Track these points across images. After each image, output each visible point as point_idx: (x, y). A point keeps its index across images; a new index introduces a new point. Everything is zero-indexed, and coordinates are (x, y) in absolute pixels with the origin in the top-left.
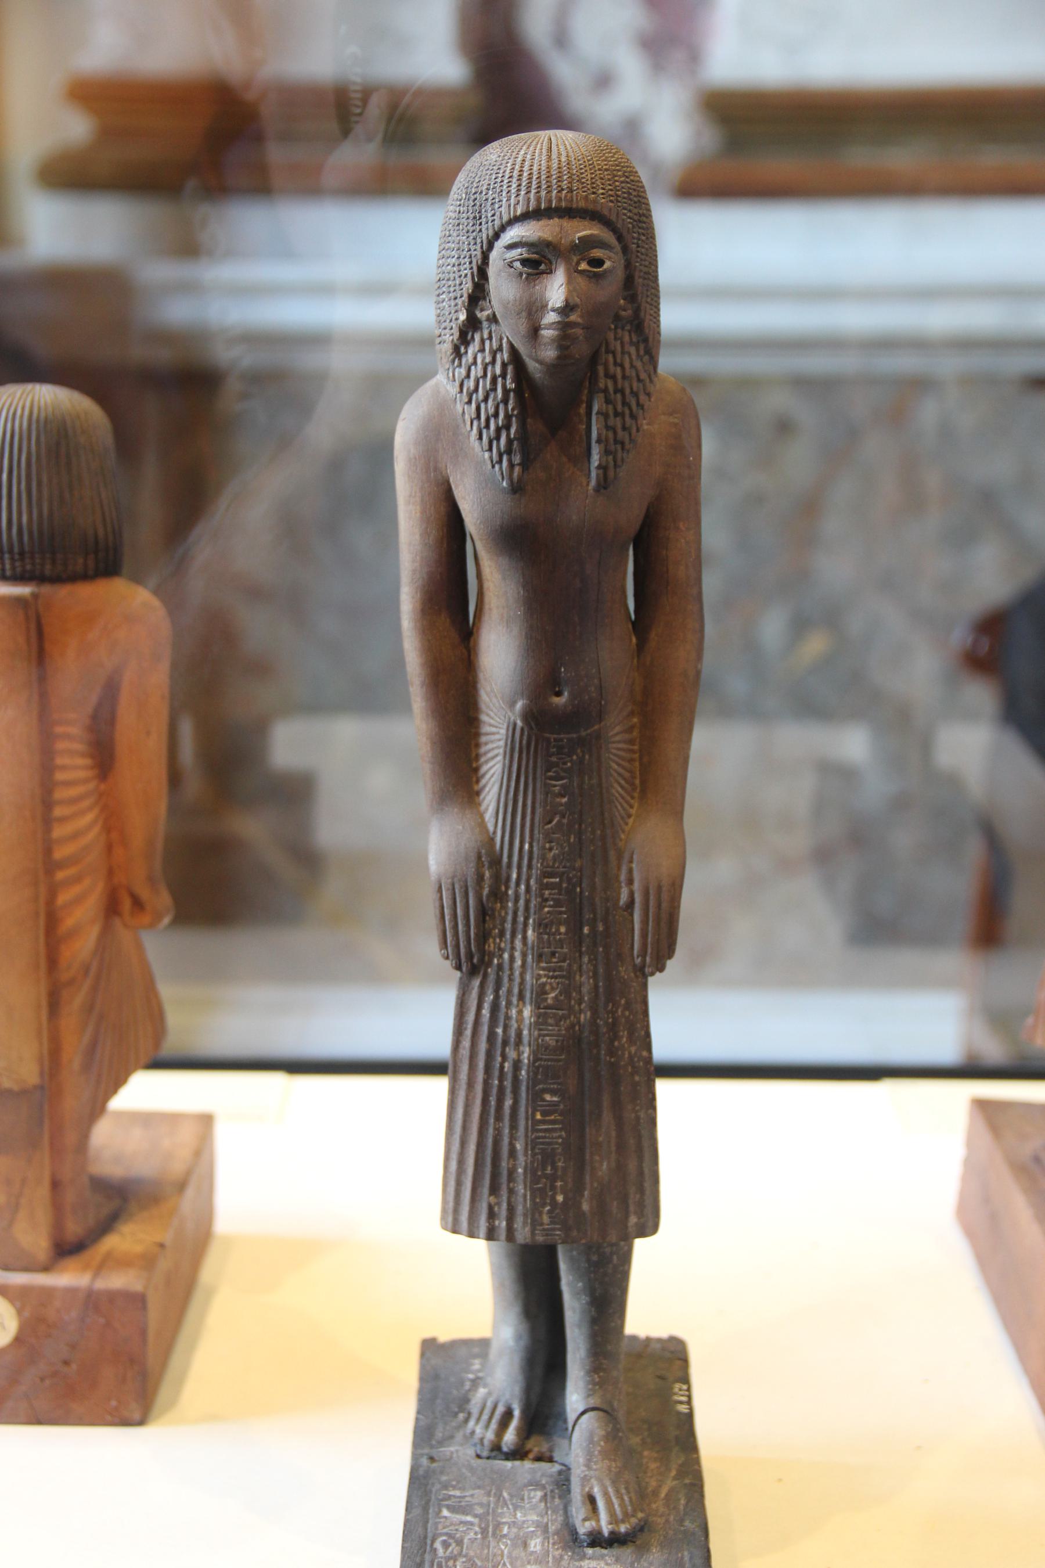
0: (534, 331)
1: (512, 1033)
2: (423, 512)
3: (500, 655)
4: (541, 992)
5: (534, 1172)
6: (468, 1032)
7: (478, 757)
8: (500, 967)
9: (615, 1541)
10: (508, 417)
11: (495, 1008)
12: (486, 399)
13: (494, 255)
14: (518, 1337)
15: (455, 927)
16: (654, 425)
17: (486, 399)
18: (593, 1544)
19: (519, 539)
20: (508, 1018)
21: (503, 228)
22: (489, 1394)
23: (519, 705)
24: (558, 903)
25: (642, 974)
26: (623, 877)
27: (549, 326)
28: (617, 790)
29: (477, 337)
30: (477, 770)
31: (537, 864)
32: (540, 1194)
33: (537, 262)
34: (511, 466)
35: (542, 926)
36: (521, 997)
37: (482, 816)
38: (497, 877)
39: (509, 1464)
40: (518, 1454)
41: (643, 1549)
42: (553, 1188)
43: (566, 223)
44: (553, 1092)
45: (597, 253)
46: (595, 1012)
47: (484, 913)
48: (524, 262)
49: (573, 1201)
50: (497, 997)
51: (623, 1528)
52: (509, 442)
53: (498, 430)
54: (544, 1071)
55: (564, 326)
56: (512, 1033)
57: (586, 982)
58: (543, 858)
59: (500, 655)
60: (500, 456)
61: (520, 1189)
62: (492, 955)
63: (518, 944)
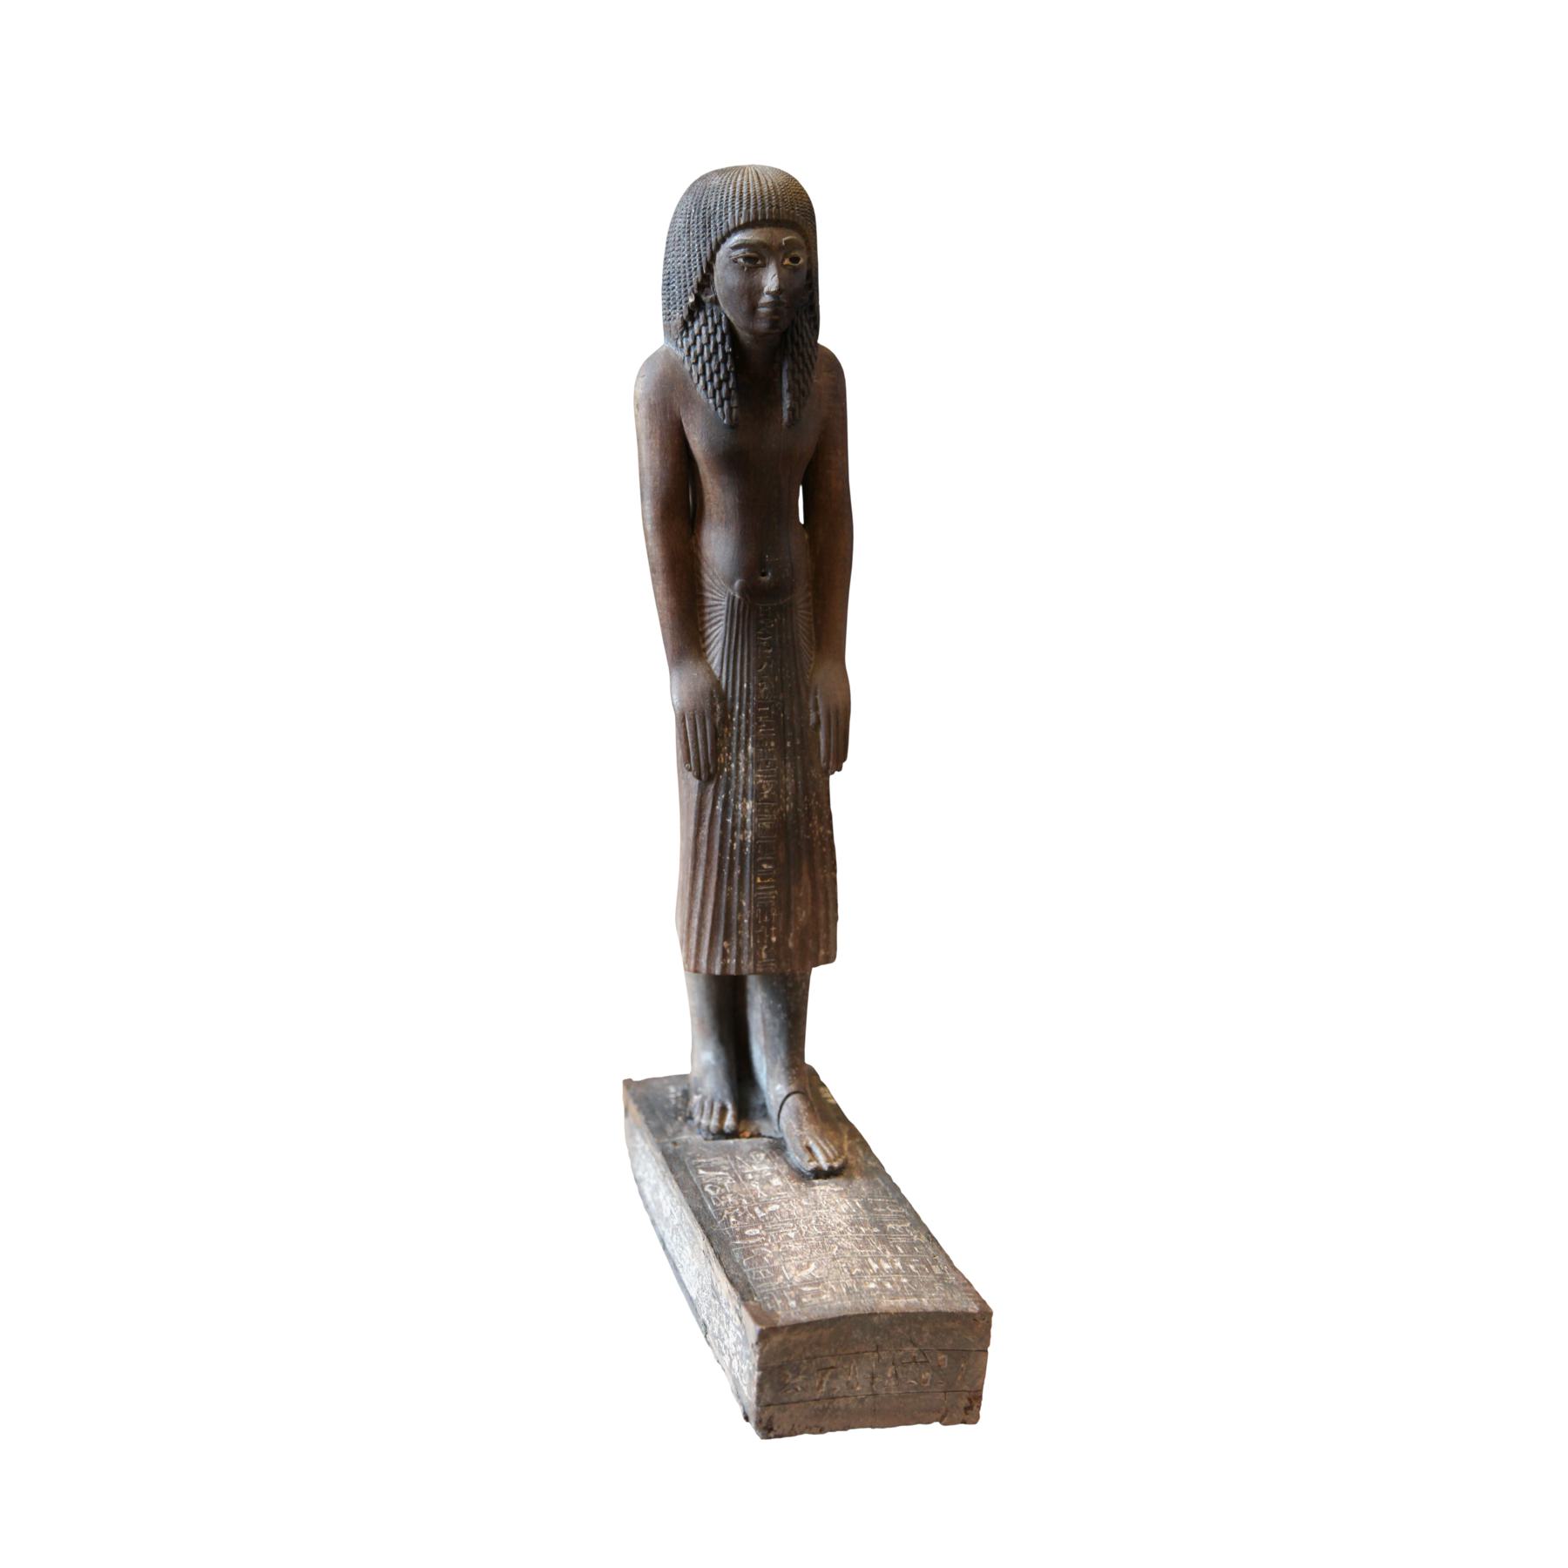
0: (753, 309)
1: (739, 821)
2: (662, 444)
3: (718, 547)
4: (758, 792)
5: (756, 921)
6: (706, 823)
7: (703, 623)
8: (729, 774)
9: (831, 1174)
10: (727, 373)
11: (726, 804)
12: (710, 361)
13: (721, 254)
14: (717, 1058)
15: (696, 746)
17: (710, 361)
18: (817, 1177)
19: (734, 461)
20: (735, 810)
21: (729, 234)
22: (704, 1098)
23: (737, 584)
24: (769, 725)
25: (827, 773)
26: (811, 705)
27: (765, 305)
28: (803, 643)
29: (702, 316)
30: (702, 633)
31: (753, 698)
32: (760, 937)
33: (754, 259)
34: (730, 408)
35: (758, 743)
36: (745, 795)
37: (709, 665)
38: (724, 709)
39: (731, 1142)
40: (735, 1134)
41: (850, 1178)
42: (769, 932)
43: (776, 232)
44: (769, 862)
45: (797, 253)
46: (796, 803)
47: (716, 736)
48: (746, 258)
49: (782, 942)
50: (727, 796)
51: (836, 1165)
52: (729, 390)
53: (720, 382)
54: (760, 847)
55: (772, 305)
56: (739, 821)
57: (789, 781)
58: (757, 693)
59: (718, 547)
60: (722, 400)
61: (746, 934)
62: (723, 765)
63: (741, 756)
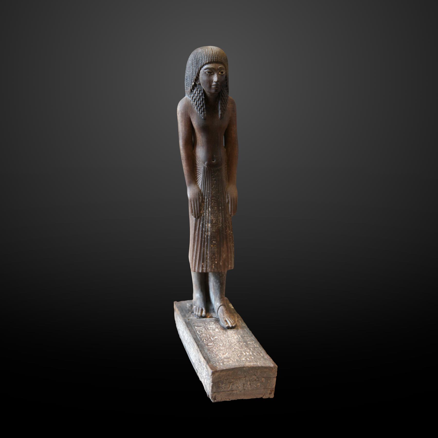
0: (210, 86)
1: (206, 229)
2: (185, 124)
4: (212, 221)
5: (211, 257)
6: (197, 230)
7: (196, 174)
8: (204, 216)
9: (232, 328)
10: (203, 104)
11: (203, 225)
12: (198, 101)
13: (201, 71)
14: (200, 296)
15: (195, 208)
16: (229, 106)
17: (198, 101)
18: (228, 329)
19: (205, 129)
20: (205, 226)
21: (204, 65)
22: (197, 307)
23: (206, 163)
24: (215, 203)
26: (227, 197)
27: (214, 85)
28: (224, 180)
29: (196, 88)
30: (196, 177)
31: (210, 195)
32: (212, 262)
33: (211, 72)
34: (204, 114)
35: (212, 208)
36: (208, 222)
37: (198, 186)
38: (202, 198)
39: (204, 319)
40: (205, 317)
41: (237, 329)
42: (215, 260)
43: (217, 65)
44: (215, 241)
45: (223, 71)
46: (222, 224)
47: (200, 206)
48: (208, 72)
49: (218, 263)
50: (203, 222)
51: (233, 325)
52: (204, 109)
53: (201, 107)
54: (212, 237)
55: (216, 85)
56: (206, 229)
57: (220, 218)
58: (212, 194)
59: (201, 153)
60: (202, 112)
61: (208, 261)
62: (202, 214)
63: (207, 211)
